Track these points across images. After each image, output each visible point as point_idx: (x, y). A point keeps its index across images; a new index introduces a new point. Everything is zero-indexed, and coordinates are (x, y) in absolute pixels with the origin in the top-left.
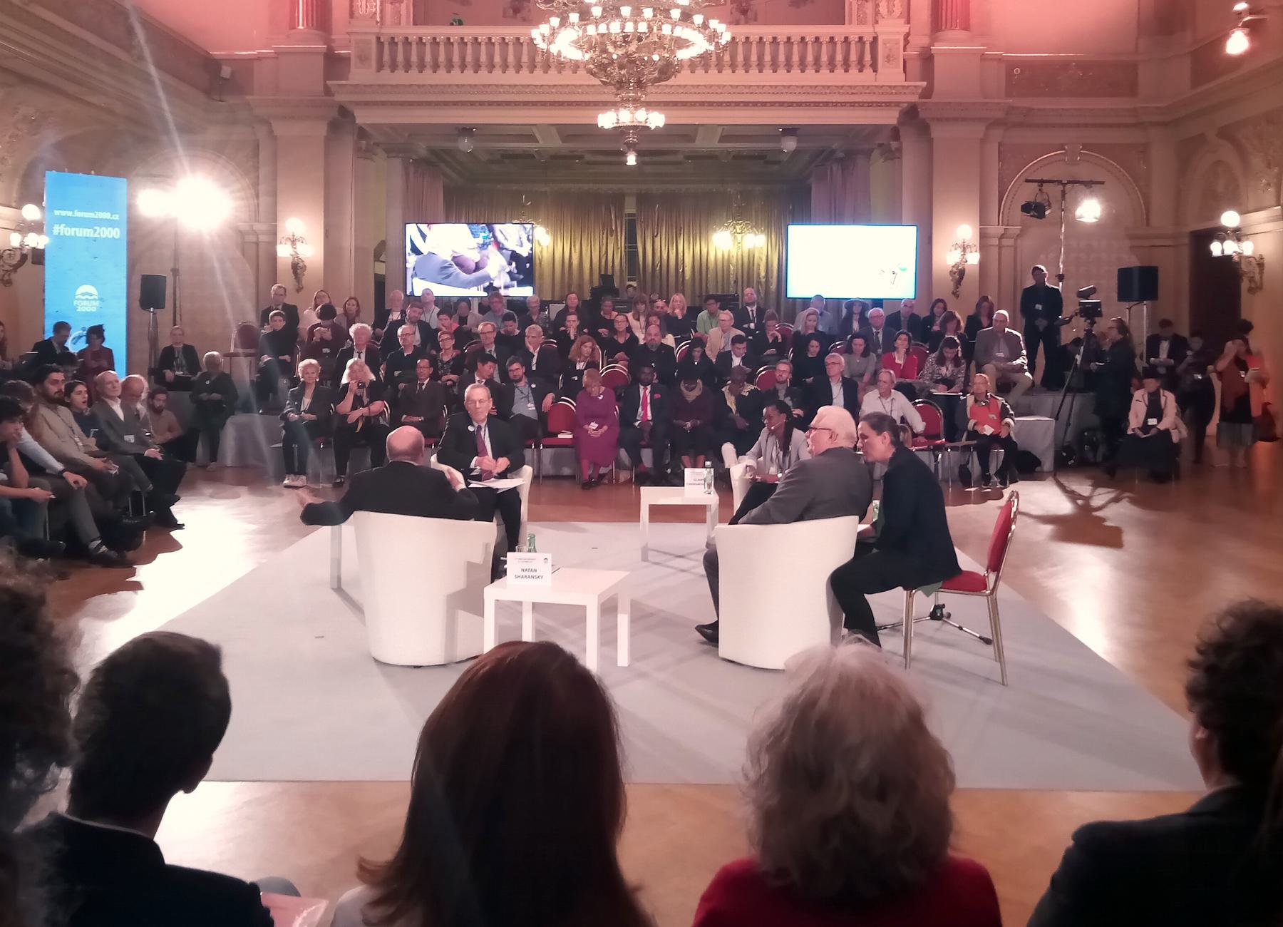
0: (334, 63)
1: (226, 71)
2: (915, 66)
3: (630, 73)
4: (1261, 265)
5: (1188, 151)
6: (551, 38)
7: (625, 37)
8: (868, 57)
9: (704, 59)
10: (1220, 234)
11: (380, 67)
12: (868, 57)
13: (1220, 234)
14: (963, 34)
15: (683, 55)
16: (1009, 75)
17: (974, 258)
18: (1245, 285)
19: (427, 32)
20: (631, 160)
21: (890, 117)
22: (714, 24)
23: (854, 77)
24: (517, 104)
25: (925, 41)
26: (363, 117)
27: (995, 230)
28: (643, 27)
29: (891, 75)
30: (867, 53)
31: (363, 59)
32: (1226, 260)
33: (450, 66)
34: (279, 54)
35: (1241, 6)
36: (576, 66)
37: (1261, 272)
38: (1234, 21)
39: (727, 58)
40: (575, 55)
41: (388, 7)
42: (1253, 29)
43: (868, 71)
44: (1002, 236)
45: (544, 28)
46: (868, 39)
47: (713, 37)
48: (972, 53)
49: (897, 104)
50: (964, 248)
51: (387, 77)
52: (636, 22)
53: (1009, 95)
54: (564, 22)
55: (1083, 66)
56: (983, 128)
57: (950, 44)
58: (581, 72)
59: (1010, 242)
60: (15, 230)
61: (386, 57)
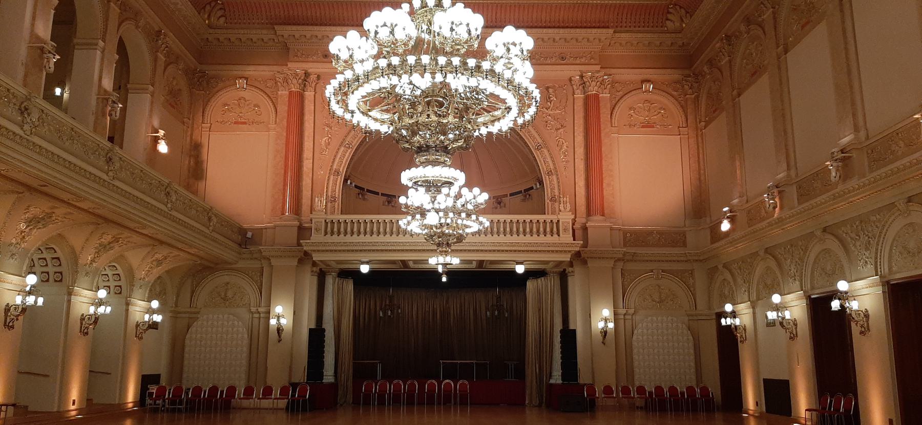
0: (303, 231)
1: (249, 235)
2: (579, 233)
3: (442, 240)
4: (867, 316)
6: (409, 223)
7: (441, 224)
8: (555, 229)
9: (479, 232)
10: (724, 315)
11: (326, 233)
12: (555, 229)
13: (724, 315)
14: (601, 218)
15: (468, 230)
16: (625, 238)
17: (611, 325)
18: (855, 329)
19: (348, 217)
21: (567, 258)
22: (481, 219)
23: (549, 239)
25: (584, 220)
26: (316, 257)
27: (622, 311)
28: (449, 221)
29: (567, 238)
30: (555, 228)
32: (728, 327)
34: (274, 227)
35: (726, 209)
36: (418, 235)
37: (867, 321)
38: (723, 216)
40: (418, 231)
41: (329, 204)
42: (732, 220)
43: (555, 236)
44: (625, 315)
45: (405, 221)
46: (555, 221)
47: (481, 223)
48: (607, 227)
49: (570, 251)
50: (606, 320)
51: (329, 239)
52: (446, 219)
53: (625, 246)
54: (413, 217)
55: (660, 233)
56: (612, 262)
57: (596, 222)
59: (629, 317)
60: (92, 304)
61: (329, 229)
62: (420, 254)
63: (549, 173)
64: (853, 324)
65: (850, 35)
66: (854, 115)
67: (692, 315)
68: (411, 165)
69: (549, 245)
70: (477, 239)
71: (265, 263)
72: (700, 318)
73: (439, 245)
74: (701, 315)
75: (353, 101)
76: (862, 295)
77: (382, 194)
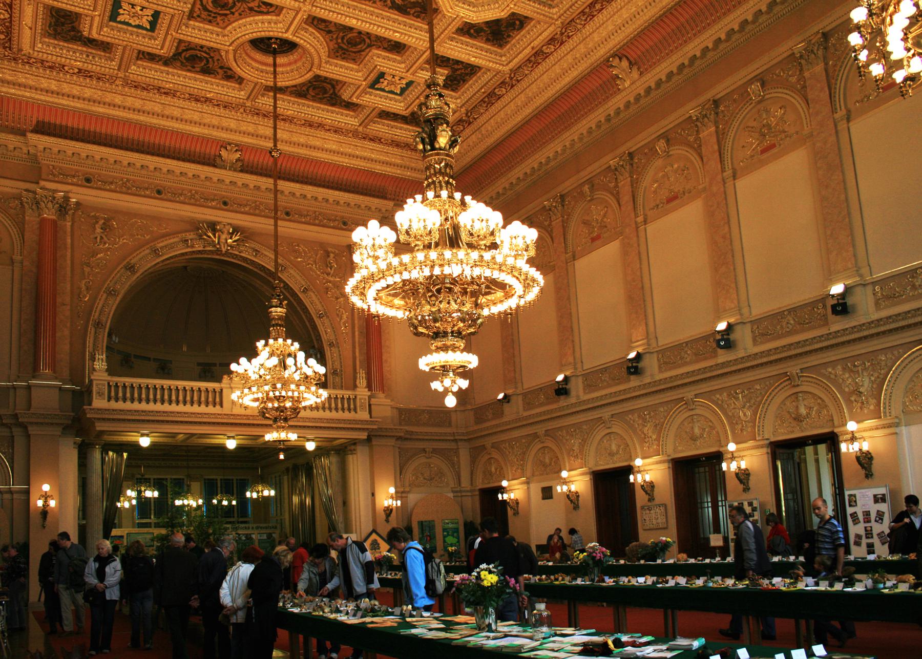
4: (518, 503)
5: (476, 453)
8: (218, 400)
10: (502, 490)
11: (109, 399)
12: (218, 400)
13: (502, 490)
20: (282, 457)
24: (195, 423)
31: (100, 394)
33: (125, 400)
39: (327, 405)
43: (353, 413)
46: (218, 390)
51: (114, 405)
53: (400, 424)
58: (308, 410)
62: (176, 427)
63: (331, 345)
64: (509, 509)
65: (644, 257)
66: (646, 324)
67: (457, 492)
68: (428, 352)
69: (321, 420)
70: (315, 414)
71: (17, 431)
72: (464, 494)
73: (275, 420)
74: (465, 491)
75: (371, 293)
76: (650, 471)
77: (154, 359)
